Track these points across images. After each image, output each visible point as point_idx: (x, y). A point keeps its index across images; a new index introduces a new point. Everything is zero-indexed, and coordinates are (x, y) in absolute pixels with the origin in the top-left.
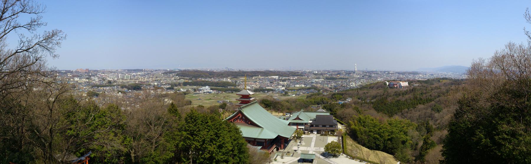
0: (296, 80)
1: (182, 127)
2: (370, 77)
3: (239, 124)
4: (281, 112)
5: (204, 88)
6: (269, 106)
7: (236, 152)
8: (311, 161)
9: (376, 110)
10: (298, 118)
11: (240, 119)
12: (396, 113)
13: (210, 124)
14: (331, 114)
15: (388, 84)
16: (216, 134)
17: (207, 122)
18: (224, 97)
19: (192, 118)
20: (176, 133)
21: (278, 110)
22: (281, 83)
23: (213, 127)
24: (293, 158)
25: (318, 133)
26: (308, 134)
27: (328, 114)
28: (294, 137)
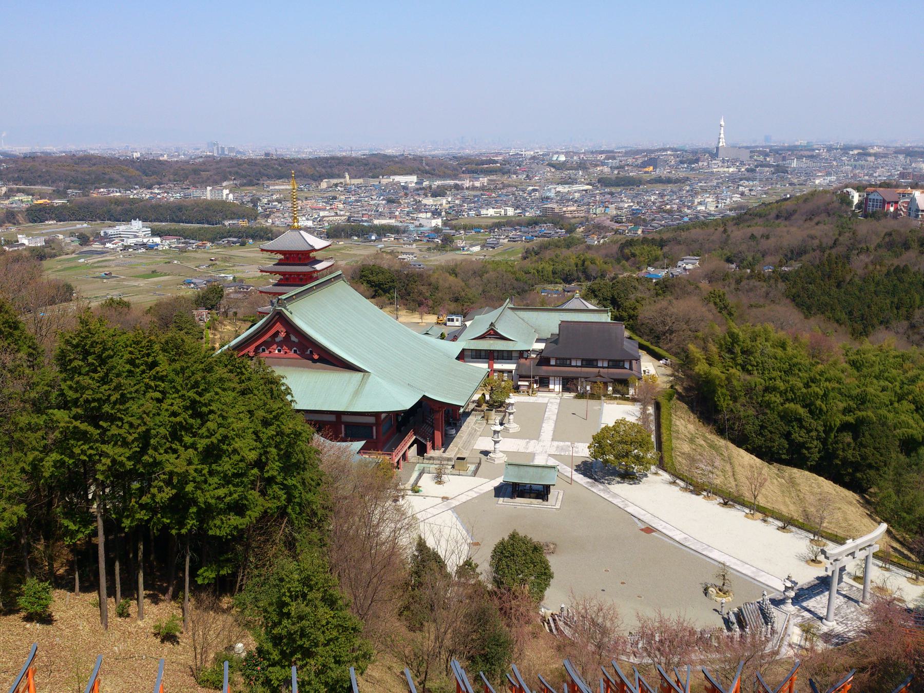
0: (483, 188)
1: (47, 394)
2: (781, 170)
3: (279, 361)
4: (432, 311)
5: (121, 228)
6: (386, 291)
7: (273, 468)
8: (542, 493)
9: (798, 305)
10: (492, 334)
11: (280, 344)
12: (885, 323)
13: (164, 368)
14: (615, 318)
15: (856, 198)
16: (194, 408)
17: (155, 364)
18: (212, 263)
19: (86, 351)
20: (23, 420)
21: (420, 304)
22: (429, 201)
23: (179, 379)
24: (477, 480)
25: (566, 389)
26: (530, 392)
27: (606, 318)
28: (479, 403)
